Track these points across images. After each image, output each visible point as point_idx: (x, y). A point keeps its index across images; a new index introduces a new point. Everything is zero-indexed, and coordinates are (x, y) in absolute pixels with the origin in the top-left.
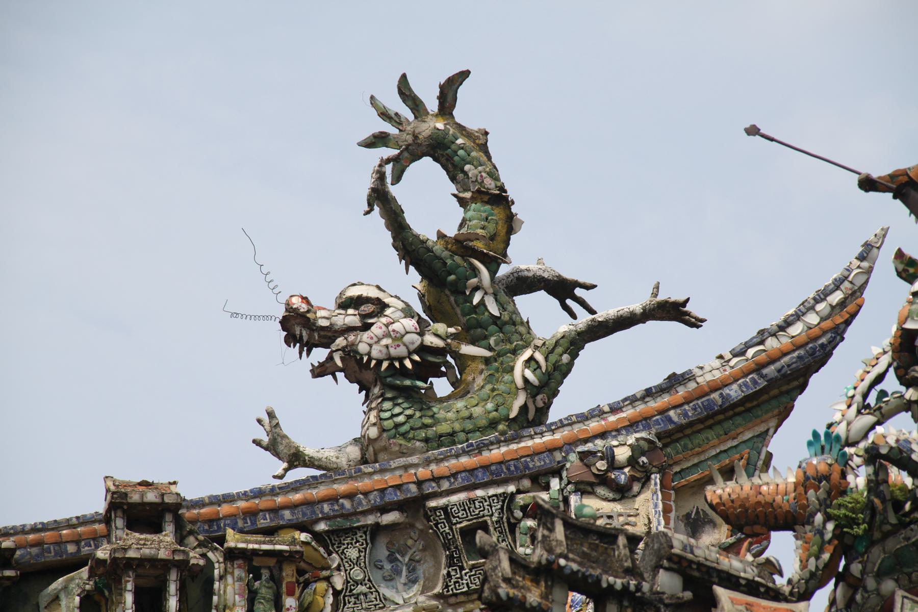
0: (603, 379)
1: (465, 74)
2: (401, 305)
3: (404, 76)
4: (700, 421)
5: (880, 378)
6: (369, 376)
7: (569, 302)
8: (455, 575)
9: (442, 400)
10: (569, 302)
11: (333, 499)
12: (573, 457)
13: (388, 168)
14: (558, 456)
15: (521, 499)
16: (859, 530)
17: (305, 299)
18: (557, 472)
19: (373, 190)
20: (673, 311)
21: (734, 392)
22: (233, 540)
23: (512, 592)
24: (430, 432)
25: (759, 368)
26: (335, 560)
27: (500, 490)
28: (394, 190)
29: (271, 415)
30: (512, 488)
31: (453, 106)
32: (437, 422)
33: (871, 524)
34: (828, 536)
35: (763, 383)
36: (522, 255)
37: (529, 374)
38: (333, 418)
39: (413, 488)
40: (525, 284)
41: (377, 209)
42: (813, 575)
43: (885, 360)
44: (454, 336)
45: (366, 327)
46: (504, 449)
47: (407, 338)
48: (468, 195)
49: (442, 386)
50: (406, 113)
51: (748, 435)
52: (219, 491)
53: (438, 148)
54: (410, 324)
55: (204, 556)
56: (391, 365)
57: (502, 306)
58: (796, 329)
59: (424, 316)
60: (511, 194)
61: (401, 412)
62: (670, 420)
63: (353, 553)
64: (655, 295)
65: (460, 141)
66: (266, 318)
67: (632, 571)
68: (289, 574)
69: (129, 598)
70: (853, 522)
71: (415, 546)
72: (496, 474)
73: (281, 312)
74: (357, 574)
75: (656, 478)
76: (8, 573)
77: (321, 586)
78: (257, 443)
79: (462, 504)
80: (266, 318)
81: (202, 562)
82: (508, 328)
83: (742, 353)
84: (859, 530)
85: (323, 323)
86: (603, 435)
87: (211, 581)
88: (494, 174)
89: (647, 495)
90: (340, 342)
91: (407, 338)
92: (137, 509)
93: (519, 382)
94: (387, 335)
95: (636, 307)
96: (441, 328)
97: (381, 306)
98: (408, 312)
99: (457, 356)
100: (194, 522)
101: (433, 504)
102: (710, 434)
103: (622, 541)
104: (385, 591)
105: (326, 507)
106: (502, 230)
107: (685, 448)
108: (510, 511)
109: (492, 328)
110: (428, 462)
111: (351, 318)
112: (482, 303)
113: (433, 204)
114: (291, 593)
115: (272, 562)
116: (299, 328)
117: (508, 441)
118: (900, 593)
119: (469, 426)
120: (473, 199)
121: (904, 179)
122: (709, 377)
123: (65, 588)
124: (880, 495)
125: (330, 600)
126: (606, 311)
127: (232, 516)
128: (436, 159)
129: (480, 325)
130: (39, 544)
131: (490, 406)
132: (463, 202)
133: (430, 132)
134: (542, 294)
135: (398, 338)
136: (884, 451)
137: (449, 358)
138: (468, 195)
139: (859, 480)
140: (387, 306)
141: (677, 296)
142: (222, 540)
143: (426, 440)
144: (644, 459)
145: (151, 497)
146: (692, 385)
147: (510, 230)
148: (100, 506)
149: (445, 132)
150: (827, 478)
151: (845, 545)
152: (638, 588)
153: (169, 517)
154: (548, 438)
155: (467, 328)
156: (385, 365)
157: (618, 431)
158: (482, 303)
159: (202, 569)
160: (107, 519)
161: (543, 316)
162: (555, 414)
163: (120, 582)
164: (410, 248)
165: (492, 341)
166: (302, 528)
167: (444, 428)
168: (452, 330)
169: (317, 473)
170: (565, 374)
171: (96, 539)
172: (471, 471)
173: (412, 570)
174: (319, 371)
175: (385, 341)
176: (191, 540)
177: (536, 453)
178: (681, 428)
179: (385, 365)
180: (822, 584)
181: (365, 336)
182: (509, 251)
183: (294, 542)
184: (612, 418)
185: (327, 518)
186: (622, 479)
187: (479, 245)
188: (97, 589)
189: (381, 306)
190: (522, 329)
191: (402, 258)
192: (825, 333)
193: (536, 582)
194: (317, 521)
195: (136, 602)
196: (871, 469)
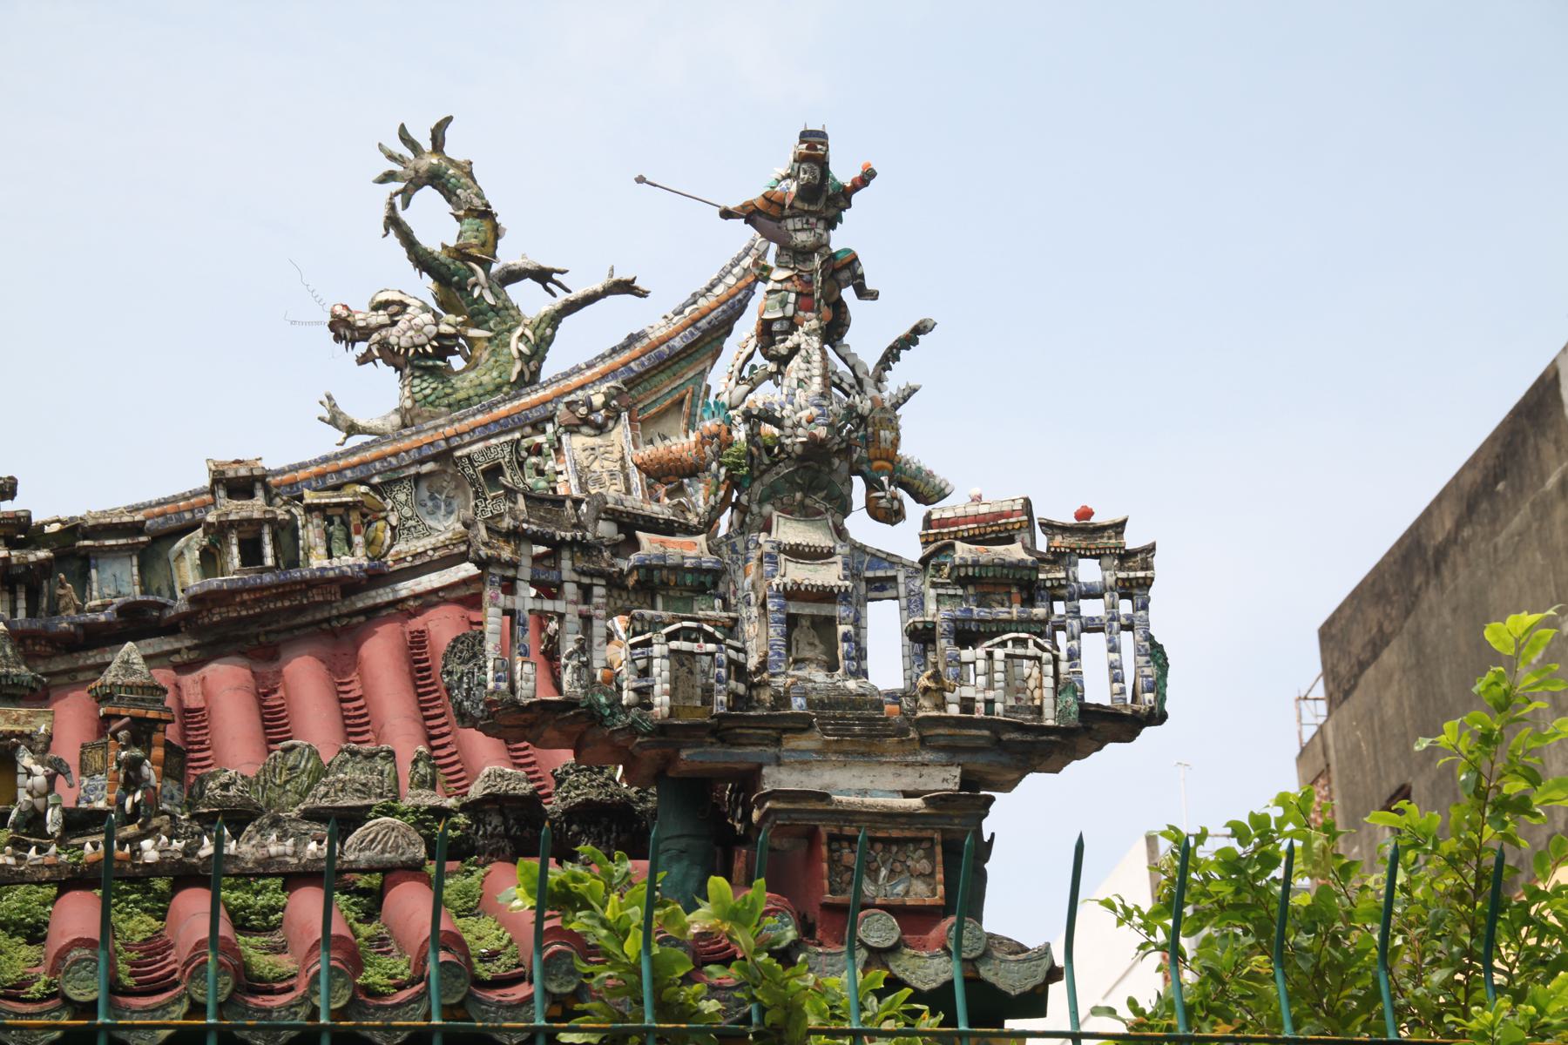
0: (580, 345)
1: (449, 120)
2: (419, 304)
3: (403, 126)
4: (654, 368)
5: (750, 356)
6: (400, 361)
7: (549, 285)
8: (481, 506)
9: (458, 373)
10: (549, 285)
11: (383, 458)
12: (561, 407)
13: (398, 200)
14: (550, 407)
15: (525, 443)
16: (744, 471)
17: (345, 307)
18: (551, 419)
19: (388, 218)
20: (625, 287)
21: (678, 343)
22: (310, 497)
23: (490, 552)
24: (452, 399)
25: (694, 322)
26: (389, 504)
27: (508, 438)
28: (403, 215)
29: (329, 398)
30: (517, 435)
31: (443, 144)
32: (456, 391)
33: (751, 466)
34: (722, 478)
35: (698, 334)
36: (508, 254)
37: (522, 347)
38: (378, 395)
39: (443, 443)
40: (513, 276)
41: (392, 231)
42: (713, 508)
43: (753, 342)
44: (463, 324)
45: (394, 323)
46: (509, 406)
47: (426, 329)
48: (461, 213)
49: (457, 362)
50: (408, 154)
51: (691, 374)
52: (296, 461)
53: (435, 179)
54: (428, 317)
55: (288, 511)
56: (416, 351)
57: (496, 296)
58: (719, 290)
59: (438, 310)
60: (494, 209)
61: (428, 386)
62: (631, 370)
63: (402, 497)
64: (611, 276)
65: (451, 172)
66: (317, 323)
67: (577, 526)
68: (355, 518)
69: (235, 550)
70: (738, 466)
71: (449, 486)
72: (504, 426)
73: (328, 319)
74: (407, 512)
75: (625, 415)
76: (143, 539)
77: (381, 524)
78: (321, 419)
79: (481, 452)
80: (317, 323)
81: (287, 517)
82: (503, 313)
83: (681, 312)
84: (744, 471)
85: (361, 324)
86: (582, 387)
87: (296, 529)
88: (480, 195)
89: (619, 429)
90: (375, 337)
91: (426, 329)
92: (236, 483)
93: (516, 354)
94: (411, 328)
95: (598, 287)
96: (451, 318)
97: (404, 306)
98: (425, 308)
99: (466, 338)
100: (278, 486)
101: (458, 453)
102: (663, 376)
103: (568, 504)
104: (430, 522)
105: (378, 465)
106: (491, 238)
107: (645, 389)
108: (518, 452)
109: (491, 314)
110: (452, 422)
111: (382, 317)
112: (481, 295)
113: (435, 222)
114: (358, 532)
115: (341, 511)
116: (343, 329)
117: (511, 400)
118: (775, 514)
119: (481, 391)
120: (466, 216)
121: (751, 208)
122: (658, 334)
123: (187, 546)
124: (756, 445)
125: (389, 533)
126: (578, 292)
127: (307, 479)
128: (434, 187)
129: (481, 312)
130: (163, 514)
131: (495, 374)
132: (458, 218)
133: (430, 168)
134: (528, 281)
135: (420, 330)
136: (755, 412)
137: (461, 341)
138: (461, 213)
139: (740, 434)
140: (407, 305)
141: (627, 276)
142: (301, 498)
143: (449, 405)
144: (614, 402)
145: (243, 472)
146: (646, 341)
147: (497, 237)
148: (206, 482)
149: (439, 165)
150: (717, 435)
151: (734, 482)
152: (584, 537)
153: (258, 485)
154: (541, 393)
155: (472, 316)
156: (411, 351)
157: (593, 382)
158: (481, 295)
159: (288, 522)
160: (212, 492)
161: (530, 300)
162: (546, 373)
163: (226, 537)
164: (422, 260)
165: (491, 324)
166: (361, 482)
167: (461, 395)
168: (460, 319)
169: (369, 438)
170: (549, 344)
171: (206, 507)
172: (485, 426)
173: (448, 505)
174: (364, 360)
175: (410, 333)
176: (278, 501)
177: (533, 407)
178: (640, 375)
179: (411, 351)
180: (721, 512)
181: (394, 330)
182: (498, 253)
183: (355, 494)
184: (589, 373)
185: (379, 473)
186: (600, 419)
187: (474, 252)
188: (211, 543)
189: (404, 306)
190: (513, 312)
191: (416, 266)
192: (740, 290)
193: (507, 542)
194: (372, 476)
195: (241, 552)
196: (747, 426)
